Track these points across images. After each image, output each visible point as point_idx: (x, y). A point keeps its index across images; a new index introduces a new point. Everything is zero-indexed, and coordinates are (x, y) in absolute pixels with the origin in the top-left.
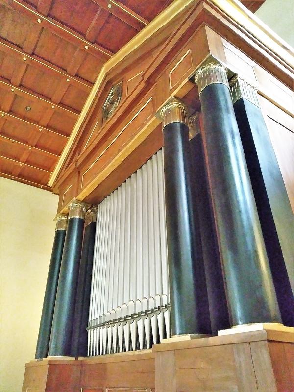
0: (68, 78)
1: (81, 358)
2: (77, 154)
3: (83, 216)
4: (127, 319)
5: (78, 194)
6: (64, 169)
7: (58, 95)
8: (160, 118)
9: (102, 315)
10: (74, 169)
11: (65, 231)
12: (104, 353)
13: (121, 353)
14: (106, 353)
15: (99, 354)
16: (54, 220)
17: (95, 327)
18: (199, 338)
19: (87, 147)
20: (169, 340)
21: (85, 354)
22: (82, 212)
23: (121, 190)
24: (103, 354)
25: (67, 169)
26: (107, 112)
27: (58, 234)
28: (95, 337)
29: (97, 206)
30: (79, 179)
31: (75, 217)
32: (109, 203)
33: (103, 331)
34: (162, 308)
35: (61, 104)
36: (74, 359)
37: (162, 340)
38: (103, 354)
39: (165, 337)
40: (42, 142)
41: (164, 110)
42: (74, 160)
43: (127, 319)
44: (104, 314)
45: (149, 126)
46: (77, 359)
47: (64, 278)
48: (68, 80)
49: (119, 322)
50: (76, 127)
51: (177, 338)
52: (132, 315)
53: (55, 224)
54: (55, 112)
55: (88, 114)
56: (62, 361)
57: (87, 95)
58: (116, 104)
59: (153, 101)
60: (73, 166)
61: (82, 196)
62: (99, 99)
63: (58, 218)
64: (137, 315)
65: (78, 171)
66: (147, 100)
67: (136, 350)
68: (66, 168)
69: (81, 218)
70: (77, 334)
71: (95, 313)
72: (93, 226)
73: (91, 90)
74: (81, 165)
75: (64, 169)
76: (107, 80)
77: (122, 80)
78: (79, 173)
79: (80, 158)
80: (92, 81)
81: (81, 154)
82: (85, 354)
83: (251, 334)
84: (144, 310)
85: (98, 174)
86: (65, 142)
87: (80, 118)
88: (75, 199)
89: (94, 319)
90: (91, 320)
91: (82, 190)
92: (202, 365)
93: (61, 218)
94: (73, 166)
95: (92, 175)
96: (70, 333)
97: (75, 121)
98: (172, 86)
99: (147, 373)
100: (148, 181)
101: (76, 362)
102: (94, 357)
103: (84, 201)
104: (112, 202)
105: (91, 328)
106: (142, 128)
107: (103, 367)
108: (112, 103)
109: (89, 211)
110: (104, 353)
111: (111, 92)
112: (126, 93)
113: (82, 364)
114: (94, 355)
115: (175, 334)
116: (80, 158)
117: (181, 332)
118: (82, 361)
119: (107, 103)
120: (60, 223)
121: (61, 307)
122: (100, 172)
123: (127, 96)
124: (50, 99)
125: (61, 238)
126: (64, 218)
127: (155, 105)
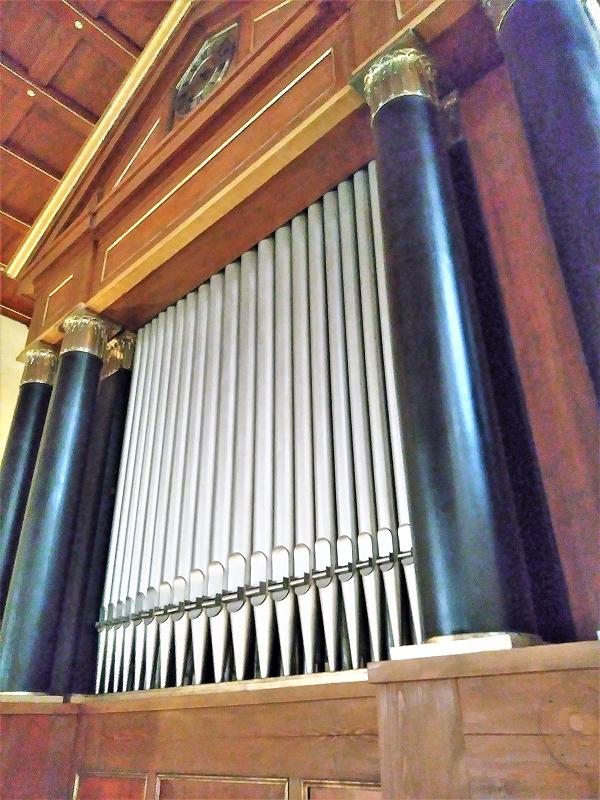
0: (81, 19)
1: (77, 699)
2: (94, 198)
3: (99, 352)
4: (224, 599)
5: (90, 293)
6: (56, 232)
7: (46, 61)
8: (363, 94)
9: (144, 590)
10: (86, 233)
11: (47, 389)
12: (148, 685)
13: (136, 693)
14: (153, 686)
15: (111, 690)
16: (18, 359)
17: (118, 622)
18: (525, 646)
19: (122, 181)
20: (420, 650)
21: (90, 690)
22: (98, 341)
23: (209, 292)
24: (142, 687)
25: (64, 234)
26: (184, 99)
27: (27, 391)
28: (114, 643)
29: (136, 332)
30: (94, 258)
31: (81, 349)
32: (162, 331)
33: (146, 632)
34: (247, 593)
35: (50, 87)
36: (59, 699)
37: (397, 652)
38: (142, 687)
39: (408, 638)
40: (15, 138)
41: (379, 67)
42: (86, 211)
43: (224, 599)
44: (150, 589)
45: (329, 109)
46: (66, 701)
47: (44, 495)
48: (79, 25)
49: (166, 613)
50: (113, 107)
51: (446, 646)
52: (240, 591)
53: (21, 367)
54: (35, 106)
55: (131, 104)
56: (30, 705)
57: (122, 75)
58: (218, 79)
59: (336, 58)
60: (83, 225)
61: (102, 299)
62: (167, 68)
63: (30, 353)
64: (388, 559)
65: (95, 239)
66: (321, 54)
67: (223, 680)
68: (60, 233)
69: (96, 353)
70: (68, 632)
71: (120, 586)
72: (125, 378)
73: (132, 63)
74: (104, 223)
75: (53, 236)
76: (198, 17)
77: (238, 19)
78: (96, 244)
79: (105, 206)
80: (138, 40)
81: (106, 198)
82: (90, 690)
83: (460, 660)
84: (212, 594)
85: (152, 245)
86: (50, 190)
87: (95, 136)
88: (83, 305)
89: (119, 602)
90: (110, 605)
91: (102, 285)
92: (577, 723)
93: (37, 354)
94: (83, 225)
95: (135, 247)
96: (51, 635)
97: (81, 139)
98: (403, 12)
99: (269, 737)
100: (370, 205)
101: (67, 710)
102: (108, 697)
103: (104, 315)
104: (181, 319)
105: (109, 624)
106: (300, 120)
107: (145, 721)
108: (205, 75)
109: (115, 341)
110: (148, 685)
111: (202, 51)
112: (250, 44)
113: (81, 713)
114: (115, 689)
115: (439, 633)
116: (105, 206)
117: (458, 627)
118: (79, 706)
119: (187, 76)
120: (32, 368)
121: (31, 564)
122: (159, 239)
123: (253, 51)
124: (25, 71)
125: (35, 405)
126: (47, 354)
127: (343, 69)
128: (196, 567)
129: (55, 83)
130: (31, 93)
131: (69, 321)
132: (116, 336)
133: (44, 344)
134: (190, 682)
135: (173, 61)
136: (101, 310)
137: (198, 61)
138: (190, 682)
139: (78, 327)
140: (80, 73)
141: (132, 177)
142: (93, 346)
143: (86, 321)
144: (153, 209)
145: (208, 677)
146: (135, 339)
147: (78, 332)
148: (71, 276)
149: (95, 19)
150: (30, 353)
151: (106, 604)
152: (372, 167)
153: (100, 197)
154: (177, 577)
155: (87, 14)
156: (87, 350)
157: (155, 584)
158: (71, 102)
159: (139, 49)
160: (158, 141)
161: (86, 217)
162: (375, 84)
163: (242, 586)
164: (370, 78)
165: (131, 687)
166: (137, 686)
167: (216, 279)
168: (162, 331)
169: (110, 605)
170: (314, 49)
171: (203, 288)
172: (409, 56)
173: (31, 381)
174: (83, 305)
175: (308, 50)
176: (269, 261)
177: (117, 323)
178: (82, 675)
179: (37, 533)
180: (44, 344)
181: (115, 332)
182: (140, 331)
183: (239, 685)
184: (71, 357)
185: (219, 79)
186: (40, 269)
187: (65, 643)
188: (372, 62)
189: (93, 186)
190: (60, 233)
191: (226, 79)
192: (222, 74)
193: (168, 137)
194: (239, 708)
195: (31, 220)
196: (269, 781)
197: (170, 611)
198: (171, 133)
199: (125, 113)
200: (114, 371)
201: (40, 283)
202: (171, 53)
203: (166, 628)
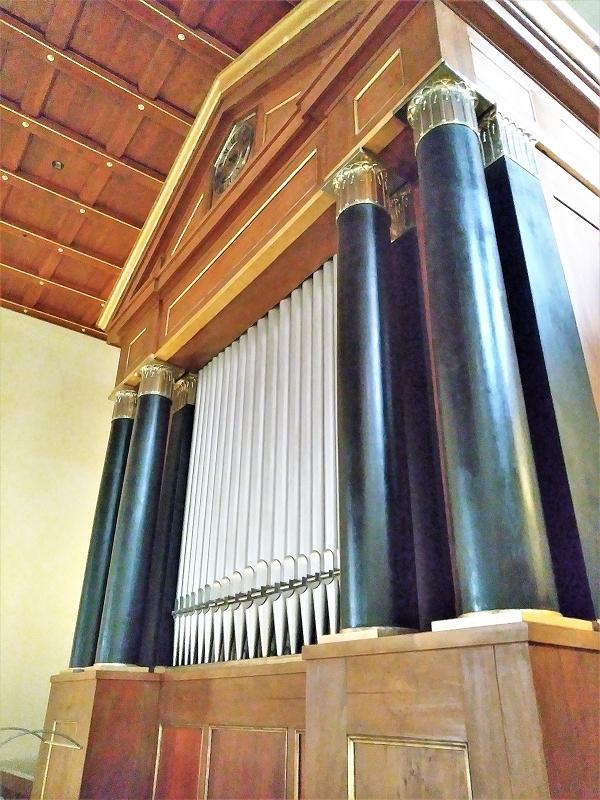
0: (82, 208)
1: (159, 670)
3: (168, 393)
7: (121, 138)
9: (203, 587)
13: (238, 662)
17: (189, 611)
19: (178, 250)
22: (166, 384)
24: (203, 661)
26: (220, 179)
27: (117, 425)
28: (188, 629)
29: (198, 373)
33: (205, 619)
35: (124, 157)
36: (146, 669)
37: (321, 638)
38: (203, 661)
39: (327, 631)
44: (207, 586)
45: (309, 209)
46: (151, 671)
47: (129, 512)
52: (264, 589)
53: (112, 405)
54: (113, 175)
57: (183, 139)
58: (241, 162)
61: (167, 350)
63: (118, 394)
65: (160, 299)
66: (307, 156)
67: (268, 656)
68: (134, 293)
69: (165, 395)
71: (189, 583)
72: (190, 411)
73: (188, 130)
74: (164, 287)
79: (165, 272)
81: (168, 261)
86: (134, 239)
88: (152, 356)
90: (181, 598)
94: (149, 289)
95: (189, 308)
96: (139, 620)
97: (154, 196)
101: (151, 677)
103: (170, 362)
105: (181, 613)
106: (295, 211)
108: (233, 159)
109: (182, 381)
112: (263, 138)
113: (162, 681)
114: (186, 663)
116: (165, 272)
120: (121, 406)
121: (121, 570)
124: (103, 147)
125: (123, 435)
126: (130, 394)
127: (322, 166)
128: (261, 558)
129: (128, 153)
130: (109, 164)
131: (144, 369)
132: (181, 378)
133: (128, 386)
134: (234, 658)
135: (211, 143)
136: (166, 359)
137: (228, 145)
138: (234, 658)
139: (151, 373)
140: (147, 143)
141: (183, 249)
142: (162, 390)
143: (157, 368)
144: (276, 193)
145: (272, 652)
146: (197, 378)
147: (150, 380)
148: (397, 52)
149: (120, 159)
150: (118, 394)
151: (178, 598)
152: (335, 257)
153: (163, 261)
154: (259, 561)
155: (148, 98)
156: (158, 393)
157: (211, 583)
158: (143, 166)
159: (192, 117)
160: (202, 217)
161: (150, 282)
162: (417, 115)
163: (318, 572)
164: (412, 108)
165: (196, 662)
166: (200, 661)
167: (251, 330)
168: (205, 378)
169: (181, 598)
170: (269, 188)
171: (305, 285)
172: (364, 167)
173: (119, 417)
174: (152, 356)
175: (283, 168)
176: (287, 319)
177: (181, 367)
178: (164, 653)
179: (125, 543)
180: (128, 386)
181: (181, 375)
182: (200, 372)
183: (252, 661)
184: (145, 401)
185: (244, 162)
186: (120, 325)
187: (470, 564)
188: (413, 93)
189: (156, 253)
190: (134, 293)
191: (252, 161)
192: (245, 157)
193: (206, 216)
194: (261, 678)
195: (122, 263)
196: (276, 730)
197: (253, 597)
198: (211, 210)
199: (177, 189)
200: (182, 406)
201: (124, 333)
202: (208, 138)
203: (278, 606)
